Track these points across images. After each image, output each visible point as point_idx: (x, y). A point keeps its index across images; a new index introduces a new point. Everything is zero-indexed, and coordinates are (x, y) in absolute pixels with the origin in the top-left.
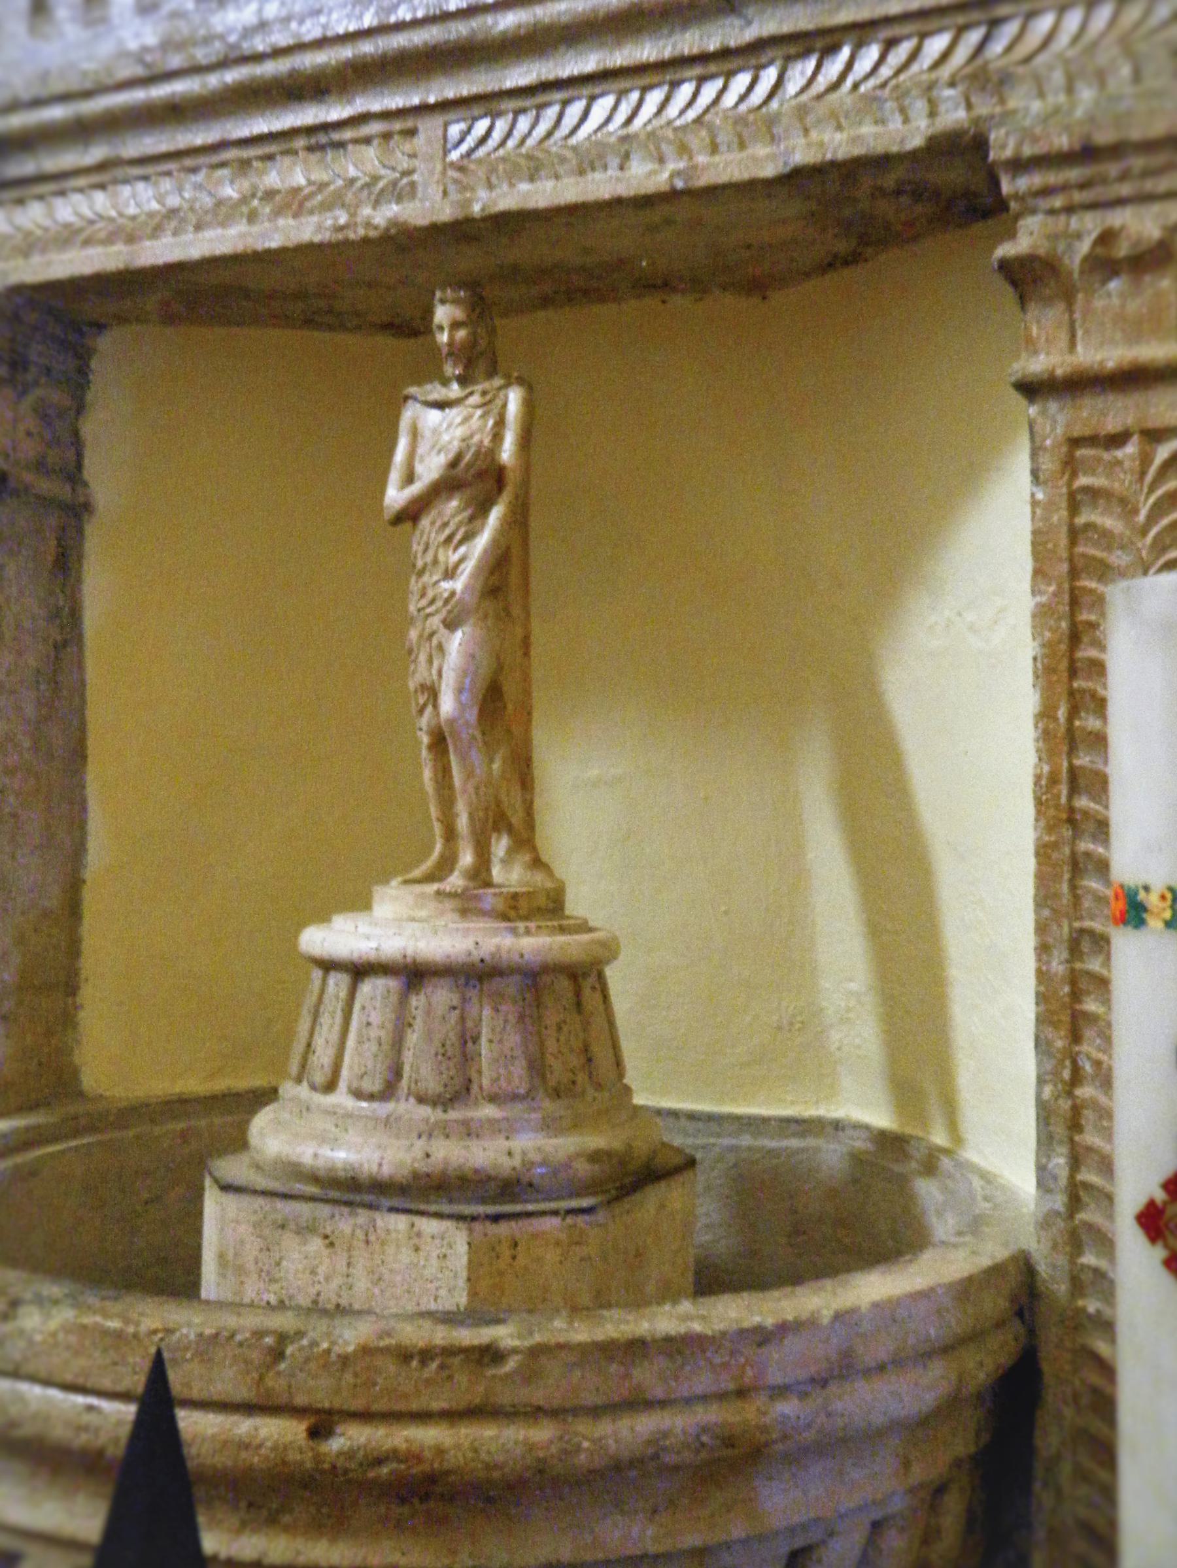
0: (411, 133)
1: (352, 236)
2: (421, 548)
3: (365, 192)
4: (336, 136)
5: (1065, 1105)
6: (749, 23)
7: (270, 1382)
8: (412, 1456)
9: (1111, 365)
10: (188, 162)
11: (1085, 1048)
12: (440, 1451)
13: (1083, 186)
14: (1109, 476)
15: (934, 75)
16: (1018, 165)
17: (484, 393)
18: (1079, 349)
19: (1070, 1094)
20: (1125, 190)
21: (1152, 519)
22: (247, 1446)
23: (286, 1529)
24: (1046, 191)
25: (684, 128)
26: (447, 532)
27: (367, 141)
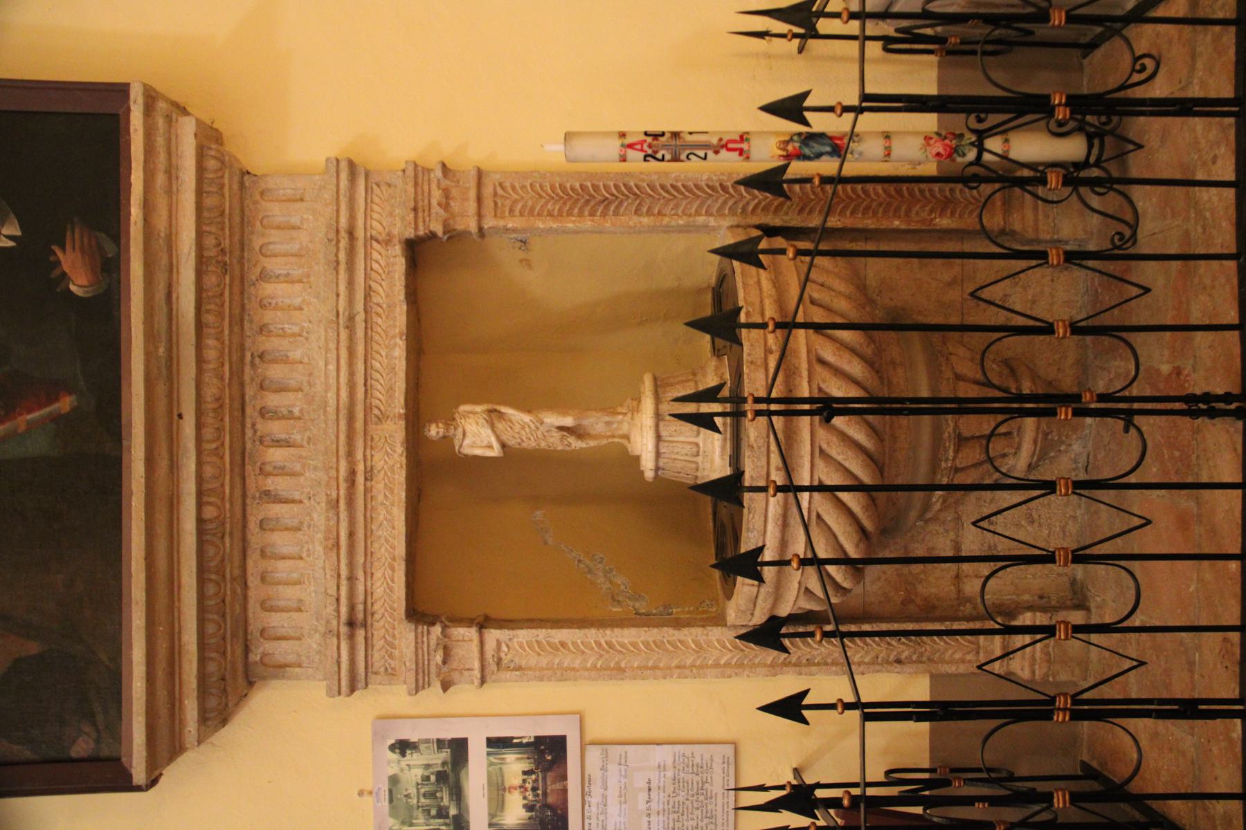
0: (372, 439)
1: (405, 462)
5: (684, 218)
10: (369, 533)
11: (668, 213)
16: (416, 228)
21: (518, 194)
23: (799, 364)
24: (424, 222)
26: (509, 429)
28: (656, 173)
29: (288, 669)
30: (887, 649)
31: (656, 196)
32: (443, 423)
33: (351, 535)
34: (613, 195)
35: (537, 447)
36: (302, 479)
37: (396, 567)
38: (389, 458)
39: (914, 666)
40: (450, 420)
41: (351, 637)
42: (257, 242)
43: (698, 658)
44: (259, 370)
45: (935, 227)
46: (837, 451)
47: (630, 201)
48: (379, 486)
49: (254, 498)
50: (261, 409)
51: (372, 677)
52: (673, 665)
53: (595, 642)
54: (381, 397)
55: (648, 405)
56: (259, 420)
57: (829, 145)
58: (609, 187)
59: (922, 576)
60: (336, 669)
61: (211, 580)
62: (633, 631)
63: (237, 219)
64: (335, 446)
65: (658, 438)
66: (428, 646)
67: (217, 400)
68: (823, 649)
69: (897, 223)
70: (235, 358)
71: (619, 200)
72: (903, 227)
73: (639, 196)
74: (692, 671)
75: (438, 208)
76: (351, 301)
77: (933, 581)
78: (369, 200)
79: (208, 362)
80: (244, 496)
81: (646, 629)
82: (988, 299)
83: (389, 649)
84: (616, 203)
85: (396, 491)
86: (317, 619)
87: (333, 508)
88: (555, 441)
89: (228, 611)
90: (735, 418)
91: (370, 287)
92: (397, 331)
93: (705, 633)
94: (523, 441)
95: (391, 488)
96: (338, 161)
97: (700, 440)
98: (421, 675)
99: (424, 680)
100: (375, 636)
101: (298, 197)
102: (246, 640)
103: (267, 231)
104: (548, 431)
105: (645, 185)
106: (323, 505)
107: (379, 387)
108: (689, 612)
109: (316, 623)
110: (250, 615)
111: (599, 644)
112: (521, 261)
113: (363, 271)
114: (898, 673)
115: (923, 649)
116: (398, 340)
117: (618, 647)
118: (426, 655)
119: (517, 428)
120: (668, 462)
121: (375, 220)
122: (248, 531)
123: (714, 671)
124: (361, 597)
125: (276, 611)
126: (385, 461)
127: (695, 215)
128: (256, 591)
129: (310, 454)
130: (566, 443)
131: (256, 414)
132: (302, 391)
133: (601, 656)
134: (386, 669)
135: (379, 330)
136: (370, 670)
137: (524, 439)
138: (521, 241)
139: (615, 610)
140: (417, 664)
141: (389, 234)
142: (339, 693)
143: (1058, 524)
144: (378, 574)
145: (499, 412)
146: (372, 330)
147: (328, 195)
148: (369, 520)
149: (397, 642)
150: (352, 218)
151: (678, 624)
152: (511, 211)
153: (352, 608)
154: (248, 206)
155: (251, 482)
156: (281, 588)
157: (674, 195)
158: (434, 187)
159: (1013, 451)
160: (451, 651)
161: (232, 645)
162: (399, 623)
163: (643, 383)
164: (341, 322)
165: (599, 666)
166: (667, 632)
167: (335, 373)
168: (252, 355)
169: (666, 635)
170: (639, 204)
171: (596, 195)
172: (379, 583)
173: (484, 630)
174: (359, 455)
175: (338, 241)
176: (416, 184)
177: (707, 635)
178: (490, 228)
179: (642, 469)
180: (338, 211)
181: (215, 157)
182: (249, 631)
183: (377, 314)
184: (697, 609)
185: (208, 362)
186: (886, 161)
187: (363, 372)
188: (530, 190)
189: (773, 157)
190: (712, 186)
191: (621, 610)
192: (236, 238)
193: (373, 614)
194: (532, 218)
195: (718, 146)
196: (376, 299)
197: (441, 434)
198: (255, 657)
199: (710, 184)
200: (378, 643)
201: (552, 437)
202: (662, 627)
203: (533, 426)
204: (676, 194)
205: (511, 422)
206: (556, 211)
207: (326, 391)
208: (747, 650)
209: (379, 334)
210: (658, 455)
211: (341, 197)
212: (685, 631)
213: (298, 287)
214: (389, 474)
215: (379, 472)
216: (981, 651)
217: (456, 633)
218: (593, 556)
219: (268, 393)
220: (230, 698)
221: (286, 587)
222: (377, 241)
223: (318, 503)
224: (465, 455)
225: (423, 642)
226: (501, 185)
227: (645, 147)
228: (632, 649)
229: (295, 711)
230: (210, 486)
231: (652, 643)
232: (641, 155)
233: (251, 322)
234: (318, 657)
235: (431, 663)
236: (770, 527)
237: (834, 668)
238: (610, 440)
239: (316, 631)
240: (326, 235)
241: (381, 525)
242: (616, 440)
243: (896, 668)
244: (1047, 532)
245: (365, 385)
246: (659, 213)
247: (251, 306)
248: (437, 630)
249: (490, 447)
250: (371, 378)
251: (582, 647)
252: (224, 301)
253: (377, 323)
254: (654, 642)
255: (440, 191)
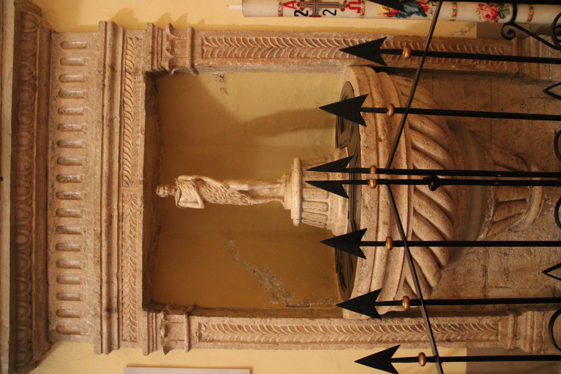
0: (123, 195)
1: (143, 211)
2: (211, 198)
3: (134, 207)
4: (121, 214)
5: (321, 60)
6: (116, 117)
7: (372, 148)
8: (383, 124)
9: (190, 50)
10: (120, 255)
11: (310, 57)
12: (381, 120)
13: (158, 55)
14: (209, 52)
15: (133, 82)
16: (152, 65)
17: (179, 184)
18: (186, 56)
19: (319, 59)
20: (160, 48)
21: (216, 44)
22: (384, 152)
24: (158, 61)
25: (133, 131)
26: (208, 191)
27: (123, 206)
28: (303, 32)
29: (72, 335)
30: (442, 333)
31: (303, 46)
32: (168, 187)
33: (109, 255)
34: (276, 45)
35: (226, 203)
36: (81, 220)
37: (137, 276)
38: (133, 208)
39: (458, 343)
40: (172, 184)
41: (109, 318)
42: (58, 74)
43: (324, 337)
44: (56, 152)
45: (476, 70)
46: (426, 211)
47: (287, 49)
48: (127, 225)
49: (53, 231)
50: (57, 176)
51: (122, 343)
52: (309, 341)
53: (260, 326)
54: (128, 169)
55: (296, 178)
56: (56, 182)
57: (417, 7)
58: (274, 40)
59: (463, 287)
60: (100, 337)
61: (22, 281)
62: (284, 320)
63: (45, 58)
64: (99, 200)
65: (302, 199)
66: (156, 325)
67: (28, 169)
68: (402, 333)
69: (453, 67)
70: (41, 144)
71: (280, 48)
72: (457, 69)
73: (292, 46)
74: (320, 345)
75: (167, 52)
76: (111, 110)
77: (470, 290)
78: (125, 48)
79: (22, 146)
80: (46, 229)
81: (292, 319)
82: (503, 120)
83: (133, 326)
84: (278, 50)
85: (137, 229)
86: (89, 306)
87: (98, 238)
88: (238, 200)
89: (33, 300)
90: (353, 185)
91: (124, 101)
92: (139, 128)
93: (329, 322)
94: (216, 199)
95: (134, 227)
96: (106, 23)
97: (329, 201)
98: (151, 343)
99: (153, 346)
100: (124, 319)
101: (83, 46)
102: (47, 317)
103: (64, 67)
104: (233, 193)
105: (296, 39)
106: (93, 236)
107: (128, 163)
108: (320, 306)
109: (89, 308)
110: (50, 302)
111: (262, 327)
112: (221, 89)
113: (119, 91)
114: (448, 347)
115: (464, 333)
116: (140, 134)
117: (274, 330)
118: (155, 331)
119: (213, 190)
120: (308, 215)
121: (128, 60)
122: (49, 251)
123: (334, 346)
124: (115, 294)
125: (65, 300)
126: (131, 210)
127: (328, 58)
128: (53, 288)
129: (85, 204)
130: (244, 201)
131: (55, 178)
132: (82, 165)
133: (263, 335)
134: (131, 338)
135: (129, 128)
136: (121, 338)
137: (218, 197)
138: (221, 77)
139: (274, 303)
140: (149, 336)
141: (136, 69)
142: (102, 352)
143: (545, 256)
144: (126, 280)
145: (202, 180)
146: (124, 128)
147: (100, 44)
148: (121, 246)
149: (137, 322)
150: (114, 58)
151: (312, 315)
152: (212, 55)
153: (109, 300)
154: (53, 52)
155: (51, 221)
156: (68, 286)
157: (313, 46)
158: (165, 39)
159: (526, 211)
160: (170, 328)
161: (36, 321)
162: (139, 311)
163: (293, 163)
164: (105, 122)
165: (262, 341)
166: (305, 321)
167: (100, 154)
168: (53, 142)
169: (304, 323)
170: (293, 51)
171: (266, 45)
172: (126, 286)
173: (191, 317)
174: (115, 206)
175: (105, 73)
176: (153, 37)
177: (331, 323)
178: (199, 65)
179: (292, 218)
180: (105, 54)
181: (30, 20)
182: (49, 312)
183: (128, 118)
184: (325, 303)
185: (22, 146)
186: (453, 20)
187: (118, 154)
188: (224, 41)
189: (380, 14)
190: (339, 41)
191: (278, 303)
192: (44, 70)
193: (123, 304)
194: (225, 59)
195: (343, 6)
196: (127, 108)
197: (166, 194)
198: (53, 327)
199: (337, 39)
200: (126, 322)
201: (236, 197)
202: (302, 317)
203: (223, 190)
204: (316, 45)
205: (210, 187)
206: (240, 55)
207: (95, 165)
208: (355, 333)
209: (129, 131)
210: (301, 210)
211: (108, 45)
212: (317, 320)
213: (80, 101)
214: (133, 218)
215: (127, 216)
216: (499, 334)
217: (173, 318)
218: (263, 268)
219: (61, 166)
220: (34, 353)
221: (71, 285)
222: (130, 73)
223: (90, 235)
224: (181, 207)
225: (153, 323)
226: (206, 39)
227: (295, 5)
228: (282, 330)
229: (78, 360)
230: (22, 223)
231: (295, 328)
232: (293, 11)
233: (53, 122)
234: (90, 329)
235: (158, 336)
236: (377, 262)
237: (409, 345)
238: (272, 200)
239: (89, 313)
240: (98, 69)
241: (128, 249)
242: (276, 200)
243: (447, 344)
244: (539, 260)
245: (119, 162)
246: (305, 57)
247: (53, 112)
248: (161, 316)
249: (196, 202)
250: (123, 158)
251: (251, 329)
252: (34, 109)
253: (127, 124)
254: (297, 327)
255: (168, 42)
